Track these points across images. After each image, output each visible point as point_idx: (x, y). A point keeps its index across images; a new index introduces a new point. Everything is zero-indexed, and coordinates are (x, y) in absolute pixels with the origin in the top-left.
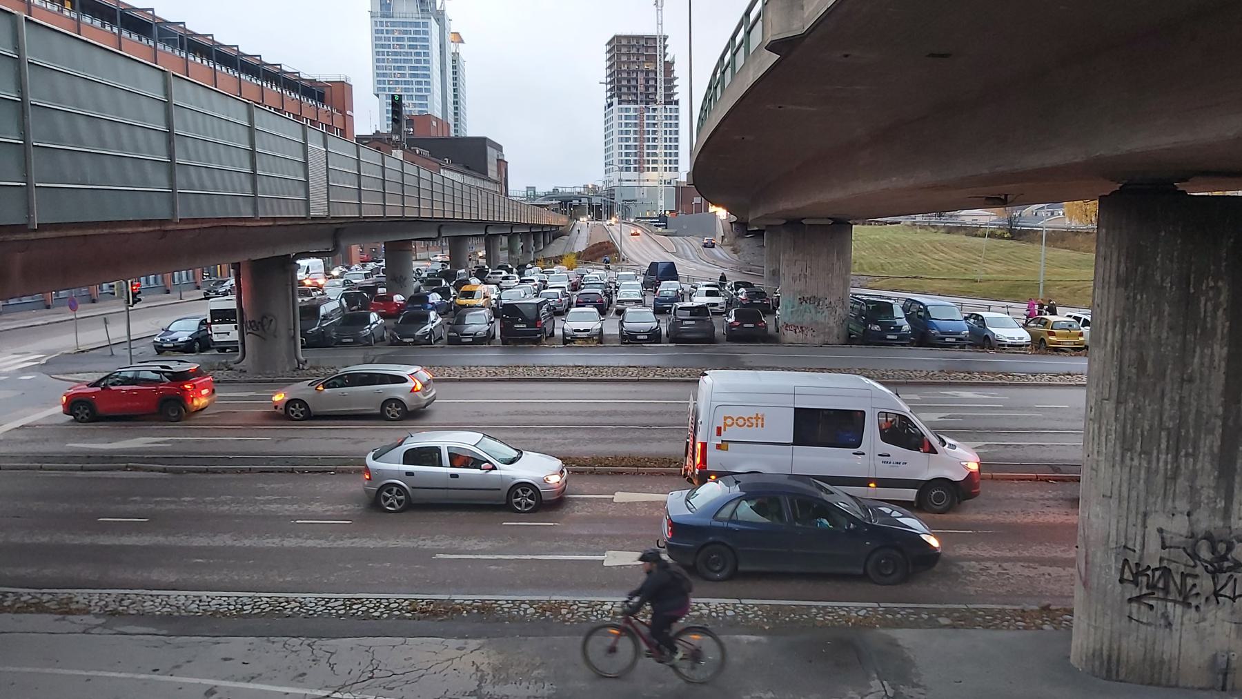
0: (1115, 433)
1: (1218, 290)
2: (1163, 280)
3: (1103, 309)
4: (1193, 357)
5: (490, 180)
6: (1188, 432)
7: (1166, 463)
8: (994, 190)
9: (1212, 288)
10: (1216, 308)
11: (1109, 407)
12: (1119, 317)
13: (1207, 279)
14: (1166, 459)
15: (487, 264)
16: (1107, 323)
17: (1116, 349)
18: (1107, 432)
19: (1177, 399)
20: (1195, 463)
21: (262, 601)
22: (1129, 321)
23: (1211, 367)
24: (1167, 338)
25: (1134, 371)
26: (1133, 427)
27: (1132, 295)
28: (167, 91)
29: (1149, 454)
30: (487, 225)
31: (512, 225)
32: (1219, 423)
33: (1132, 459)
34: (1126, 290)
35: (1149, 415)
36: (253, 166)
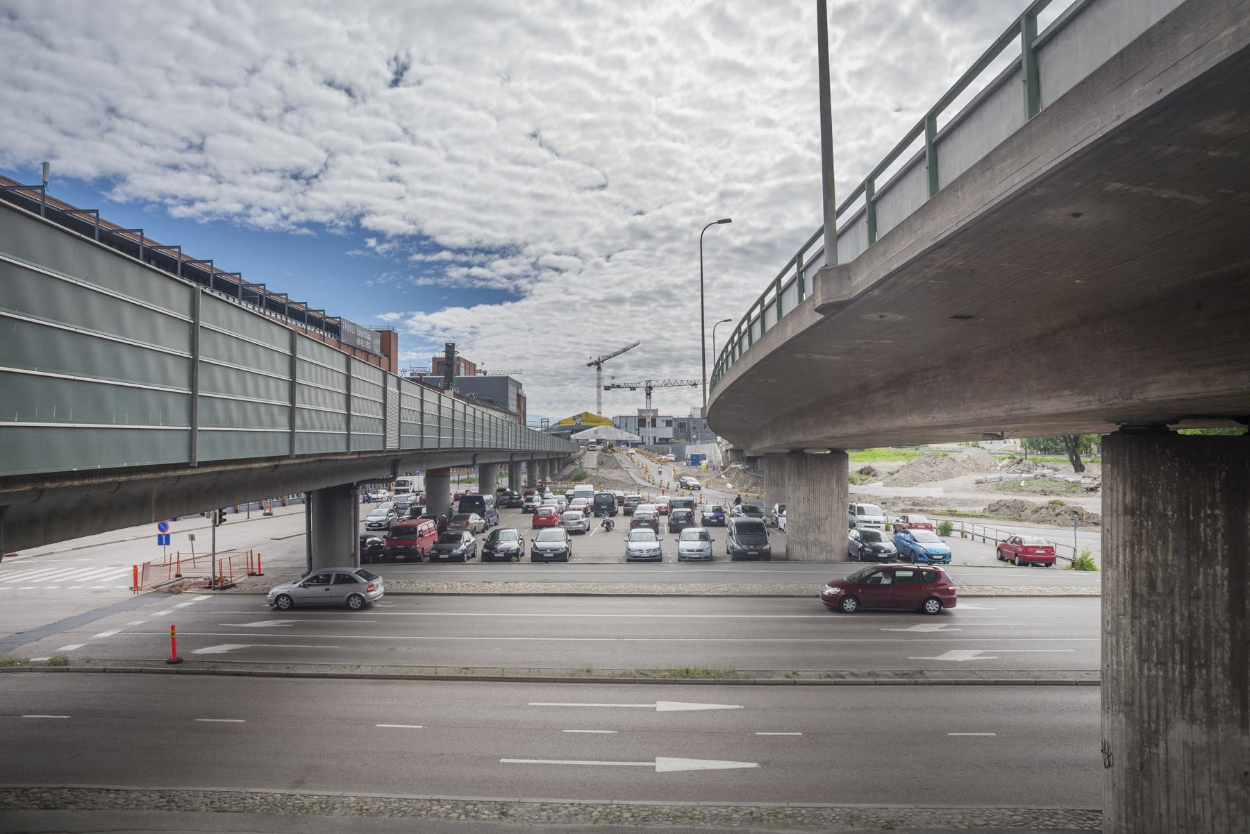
0: (1133, 645)
1: (1214, 517)
2: (1165, 509)
3: (1113, 534)
4: (1198, 577)
5: (511, 413)
6: (1199, 643)
7: (1181, 673)
8: (988, 429)
9: (1209, 516)
10: (1215, 532)
11: (1125, 621)
12: (1128, 541)
13: (1205, 508)
14: (1181, 669)
15: (509, 487)
16: (1118, 547)
17: (1127, 569)
18: (1125, 645)
19: (1186, 613)
20: (1208, 673)
21: (350, 800)
22: (1137, 544)
23: (1215, 585)
24: (1173, 560)
25: (1145, 589)
26: (1149, 640)
27: (1138, 521)
28: (293, 347)
29: (1164, 664)
30: (513, 453)
31: (534, 453)
32: (1227, 636)
33: (1149, 670)
34: (1133, 518)
35: (1161, 627)
36: (292, 398)
